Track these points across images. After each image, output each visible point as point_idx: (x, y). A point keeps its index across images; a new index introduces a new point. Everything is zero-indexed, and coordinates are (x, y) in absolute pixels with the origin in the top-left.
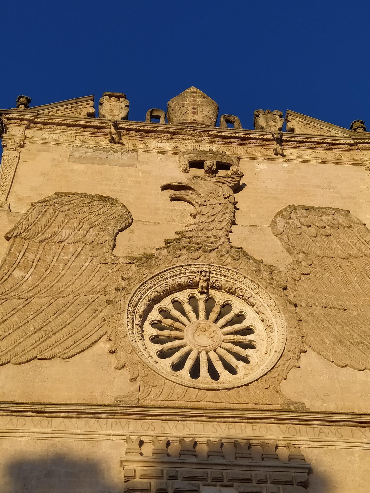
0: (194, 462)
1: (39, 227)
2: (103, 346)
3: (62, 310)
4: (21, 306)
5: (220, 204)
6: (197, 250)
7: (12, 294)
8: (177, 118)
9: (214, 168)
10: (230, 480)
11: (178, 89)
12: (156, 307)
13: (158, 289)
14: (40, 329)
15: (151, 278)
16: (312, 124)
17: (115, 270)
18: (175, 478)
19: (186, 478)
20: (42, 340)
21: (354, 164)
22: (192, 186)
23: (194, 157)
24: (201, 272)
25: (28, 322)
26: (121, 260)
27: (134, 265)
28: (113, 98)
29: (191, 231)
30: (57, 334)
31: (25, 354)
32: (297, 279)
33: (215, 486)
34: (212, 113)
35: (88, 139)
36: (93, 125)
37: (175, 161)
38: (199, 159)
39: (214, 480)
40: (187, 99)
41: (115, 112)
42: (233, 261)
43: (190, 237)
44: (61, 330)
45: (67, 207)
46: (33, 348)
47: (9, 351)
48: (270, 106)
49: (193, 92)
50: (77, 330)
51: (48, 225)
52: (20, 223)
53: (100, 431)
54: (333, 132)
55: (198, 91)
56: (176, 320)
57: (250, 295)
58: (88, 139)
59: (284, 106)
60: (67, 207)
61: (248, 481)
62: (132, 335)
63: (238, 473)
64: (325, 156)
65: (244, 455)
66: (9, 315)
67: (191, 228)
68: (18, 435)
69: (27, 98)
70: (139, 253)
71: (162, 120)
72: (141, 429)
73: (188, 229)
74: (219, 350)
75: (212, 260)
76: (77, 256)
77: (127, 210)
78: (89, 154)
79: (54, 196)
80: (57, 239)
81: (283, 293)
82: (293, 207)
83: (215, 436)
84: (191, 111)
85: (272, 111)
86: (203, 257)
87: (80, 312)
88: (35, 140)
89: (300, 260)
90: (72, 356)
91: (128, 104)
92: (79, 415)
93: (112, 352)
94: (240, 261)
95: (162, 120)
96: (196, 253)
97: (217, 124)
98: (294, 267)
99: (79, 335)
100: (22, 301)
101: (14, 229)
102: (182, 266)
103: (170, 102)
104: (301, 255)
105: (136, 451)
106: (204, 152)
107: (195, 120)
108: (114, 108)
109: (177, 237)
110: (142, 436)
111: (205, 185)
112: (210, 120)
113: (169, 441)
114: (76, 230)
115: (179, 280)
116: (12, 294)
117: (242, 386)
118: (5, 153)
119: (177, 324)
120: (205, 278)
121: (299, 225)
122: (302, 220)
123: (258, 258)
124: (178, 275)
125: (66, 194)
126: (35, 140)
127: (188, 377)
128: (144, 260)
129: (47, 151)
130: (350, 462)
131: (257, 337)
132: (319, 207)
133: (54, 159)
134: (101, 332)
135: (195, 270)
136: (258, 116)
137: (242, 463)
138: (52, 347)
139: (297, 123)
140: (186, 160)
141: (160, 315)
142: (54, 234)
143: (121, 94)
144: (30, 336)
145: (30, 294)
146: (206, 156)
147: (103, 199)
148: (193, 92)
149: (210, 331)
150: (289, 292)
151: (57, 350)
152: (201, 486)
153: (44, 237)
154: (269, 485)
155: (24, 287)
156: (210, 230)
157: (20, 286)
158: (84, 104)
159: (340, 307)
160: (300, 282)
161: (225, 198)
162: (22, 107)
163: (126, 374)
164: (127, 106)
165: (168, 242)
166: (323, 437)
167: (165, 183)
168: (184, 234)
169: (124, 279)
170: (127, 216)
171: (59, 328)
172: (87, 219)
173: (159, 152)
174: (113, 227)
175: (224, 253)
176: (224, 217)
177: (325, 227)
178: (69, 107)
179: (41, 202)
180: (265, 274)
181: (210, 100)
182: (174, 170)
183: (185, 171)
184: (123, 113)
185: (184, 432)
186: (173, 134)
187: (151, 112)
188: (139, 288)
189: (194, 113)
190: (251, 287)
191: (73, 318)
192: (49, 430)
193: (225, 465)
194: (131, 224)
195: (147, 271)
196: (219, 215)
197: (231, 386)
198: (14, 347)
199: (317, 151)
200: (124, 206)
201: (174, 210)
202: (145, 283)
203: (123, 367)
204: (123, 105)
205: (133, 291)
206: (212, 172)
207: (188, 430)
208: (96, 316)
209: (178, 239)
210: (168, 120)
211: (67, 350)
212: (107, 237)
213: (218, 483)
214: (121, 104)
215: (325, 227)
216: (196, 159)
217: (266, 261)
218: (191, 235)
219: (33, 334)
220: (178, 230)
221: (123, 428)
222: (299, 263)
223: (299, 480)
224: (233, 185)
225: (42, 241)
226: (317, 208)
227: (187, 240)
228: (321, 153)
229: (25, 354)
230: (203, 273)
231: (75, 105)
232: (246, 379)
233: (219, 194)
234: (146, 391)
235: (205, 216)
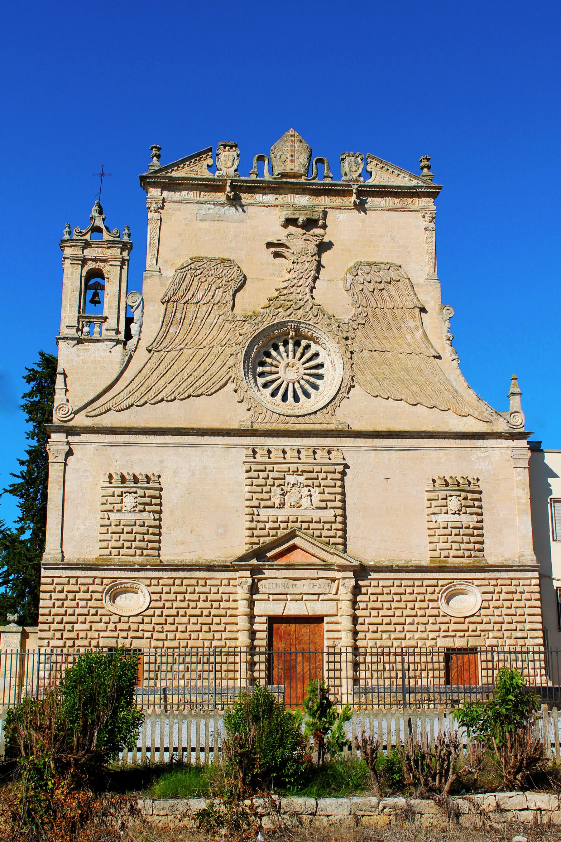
1: (181, 292)
26: (238, 318)
38: (294, 217)
49: (292, 136)
55: (296, 134)
63: (309, 468)
74: (302, 382)
78: (211, 211)
80: (195, 300)
81: (345, 343)
84: (290, 158)
98: (354, 319)
110: (229, 608)
123: (331, 313)
126: (171, 201)
129: (180, 210)
134: (228, 376)
138: (199, 388)
147: (223, 261)
148: (292, 136)
149: (295, 367)
151: (202, 390)
158: (204, 156)
164: (238, 156)
173: (264, 206)
174: (233, 286)
212: (229, 298)
216: (291, 216)
225: (185, 303)
232: (315, 406)
235: (296, 273)
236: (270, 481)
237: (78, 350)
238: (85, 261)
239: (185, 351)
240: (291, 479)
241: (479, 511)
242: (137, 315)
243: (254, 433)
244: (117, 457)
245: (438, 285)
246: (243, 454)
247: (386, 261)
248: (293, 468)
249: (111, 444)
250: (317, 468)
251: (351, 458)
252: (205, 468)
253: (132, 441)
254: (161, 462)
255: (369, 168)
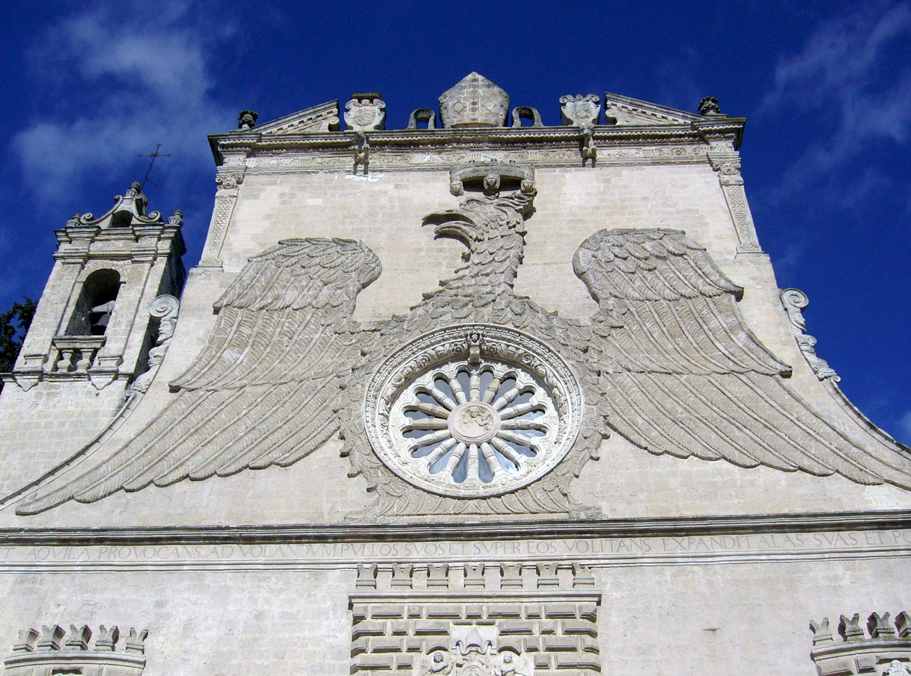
0: (444, 594)
2: (335, 446)
3: (283, 400)
4: (231, 399)
5: (502, 237)
6: (467, 305)
7: (220, 384)
8: (451, 118)
9: (498, 185)
10: (490, 616)
11: (452, 80)
12: (412, 387)
13: (413, 364)
14: (254, 428)
15: (402, 349)
16: (640, 110)
17: (353, 341)
18: (417, 616)
19: (431, 616)
20: (255, 443)
21: (698, 163)
22: (465, 214)
23: (469, 173)
24: (471, 335)
25: (239, 419)
27: (379, 333)
28: (364, 101)
29: (460, 278)
30: (276, 434)
31: (234, 462)
32: (605, 334)
33: (470, 624)
34: (498, 107)
35: (329, 161)
36: (341, 143)
37: (445, 180)
38: (476, 175)
39: (469, 617)
40: (466, 91)
41: (366, 120)
42: (514, 317)
43: (458, 288)
44: (280, 427)
45: (293, 260)
46: (245, 454)
47: (215, 459)
48: (579, 90)
50: (301, 426)
51: (269, 287)
52: (232, 287)
53: (326, 559)
54: (670, 118)
55: (480, 77)
56: (439, 402)
57: (538, 362)
58: (329, 161)
59: (601, 85)
60: (293, 260)
61: (571, 616)
62: (372, 429)
63: (504, 606)
64: (657, 154)
65: (512, 582)
66: (215, 412)
67: (461, 273)
68: (222, 567)
69: (251, 114)
70: (386, 315)
71: (431, 125)
72: (379, 553)
73: (456, 276)
75: (486, 318)
76: (305, 327)
77: (374, 255)
79: (278, 246)
80: (280, 304)
82: (604, 233)
83: (476, 559)
84: (469, 106)
85: (584, 96)
86: (473, 314)
87: (306, 402)
88: (258, 171)
89: (610, 308)
90: (293, 462)
91: (384, 106)
92: (299, 539)
93: (343, 455)
94: (524, 316)
95: (431, 125)
96: (465, 309)
97: (508, 121)
98: (601, 318)
99: (303, 435)
100: (233, 392)
101: (225, 296)
102: (445, 330)
103: (441, 97)
104: (612, 301)
105: (370, 583)
106: (484, 164)
107: (474, 119)
108: (365, 115)
109: (441, 288)
111: (483, 210)
112: (495, 118)
113: (413, 568)
114: (306, 289)
115: (514, 349)
116: (220, 384)
117: (517, 490)
118: (220, 192)
119: (439, 409)
120: (478, 343)
121: (612, 257)
122: (617, 250)
124: (439, 342)
125: (294, 242)
127: (451, 480)
128: (393, 324)
129: (274, 184)
130: (658, 582)
131: (548, 419)
132: (641, 230)
133: (282, 195)
135: (462, 334)
136: (565, 104)
137: (507, 594)
138: (269, 451)
139: (621, 111)
140: (458, 177)
141: (416, 398)
142: (277, 298)
143: (374, 94)
144: (241, 438)
145: (244, 382)
146: (486, 170)
147: (342, 243)
150: (593, 356)
152: (451, 625)
153: (263, 303)
154: (544, 620)
155: (237, 373)
156: (487, 275)
157: (232, 372)
158: (324, 113)
159: (662, 370)
160: (609, 338)
161: (510, 228)
162: (245, 126)
163: (361, 483)
165: (427, 297)
166: (624, 552)
167: (429, 213)
168: (451, 283)
169: (363, 354)
170: (373, 265)
171: (278, 426)
172: (319, 273)
175: (503, 307)
176: (508, 254)
177: (646, 259)
178: (305, 119)
179: (261, 256)
180: (559, 332)
181: (496, 89)
182: (438, 194)
183: (456, 193)
184: (378, 119)
185: (436, 555)
186: (440, 145)
187: (416, 115)
188: (385, 364)
189: (474, 110)
190: (539, 351)
191: (297, 411)
192: (262, 560)
193: (487, 597)
194: (379, 274)
195: (396, 340)
196: (501, 253)
197: (502, 491)
198: (221, 454)
199: (647, 148)
200: (370, 250)
201: (441, 250)
202: (392, 356)
203: (359, 473)
204: (376, 109)
205: (376, 369)
206: (491, 191)
207: (441, 552)
208: (326, 406)
209: (441, 292)
210: (439, 122)
211: (287, 455)
213: (474, 621)
214: (373, 108)
215: (646, 259)
216: (471, 175)
217: (562, 314)
218: (460, 285)
219: (245, 435)
220: (443, 279)
221: (356, 554)
222: (608, 312)
223: (585, 611)
224: (521, 207)
226: (639, 230)
227: (453, 292)
228: (652, 151)
229: (234, 462)
230: (475, 337)
231: (313, 116)
233: (502, 223)
234: (386, 505)
236: (410, 639)
237: (39, 395)
238: (89, 257)
239: (247, 389)
240: (458, 632)
241: (590, 658)
242: (165, 328)
243: (379, 535)
244: (61, 597)
245: (766, 258)
246: (338, 585)
247: (656, 227)
248: (464, 608)
249: (55, 569)
250: (407, 607)
251: (607, 582)
252: (259, 616)
253: (104, 559)
254: (160, 604)
255: (609, 113)
